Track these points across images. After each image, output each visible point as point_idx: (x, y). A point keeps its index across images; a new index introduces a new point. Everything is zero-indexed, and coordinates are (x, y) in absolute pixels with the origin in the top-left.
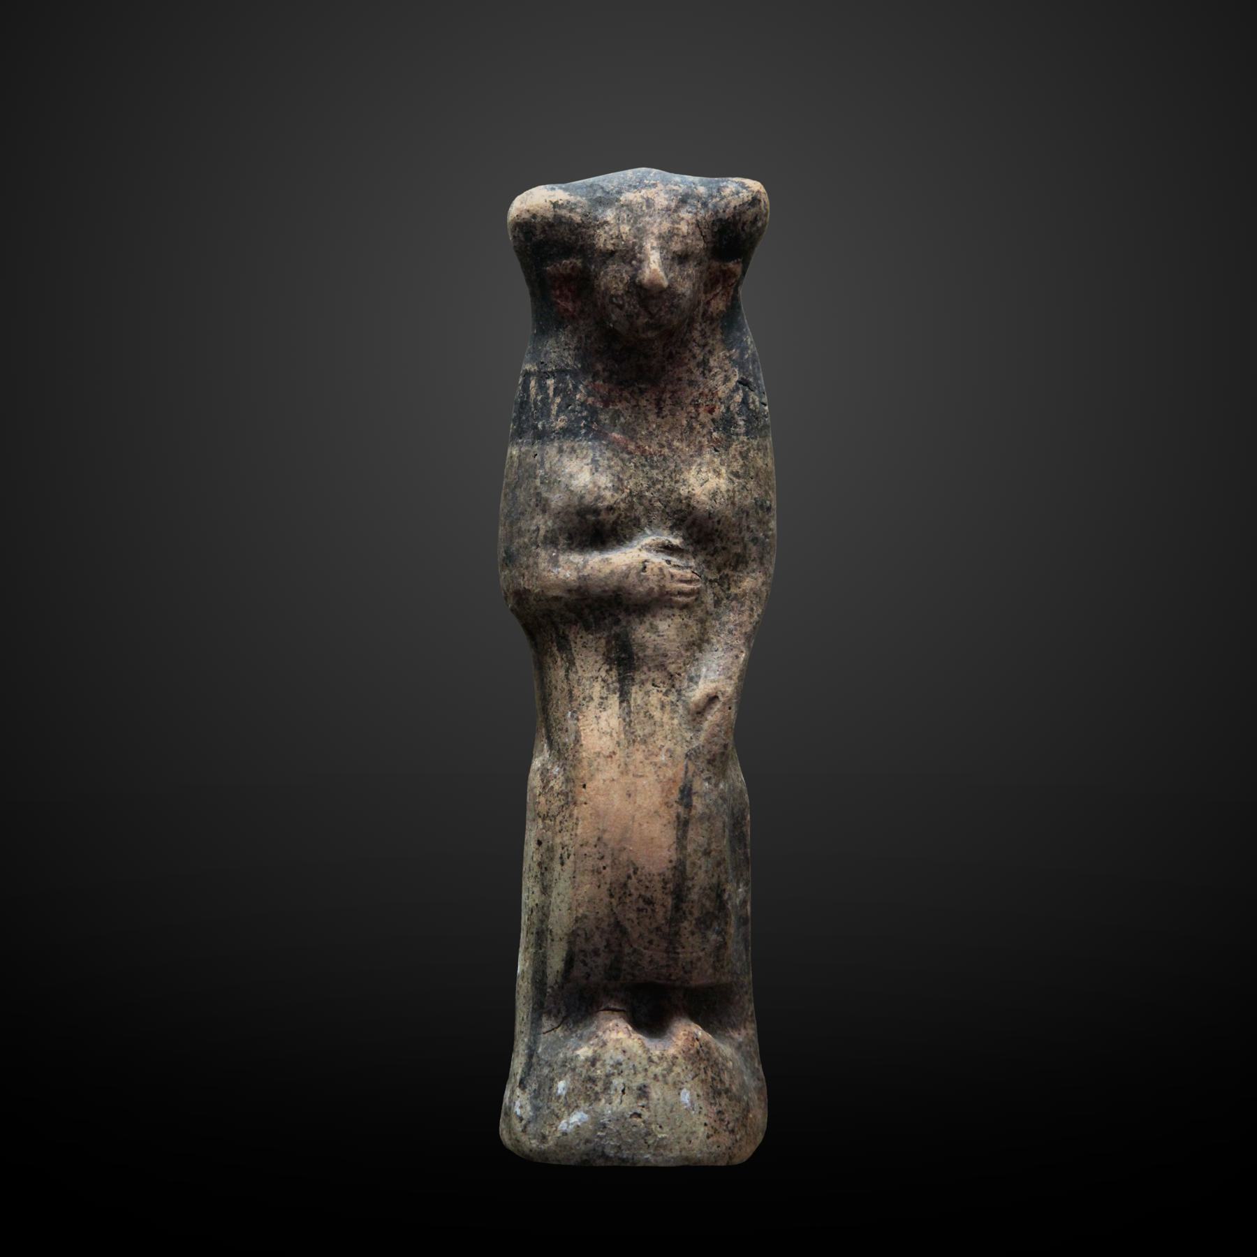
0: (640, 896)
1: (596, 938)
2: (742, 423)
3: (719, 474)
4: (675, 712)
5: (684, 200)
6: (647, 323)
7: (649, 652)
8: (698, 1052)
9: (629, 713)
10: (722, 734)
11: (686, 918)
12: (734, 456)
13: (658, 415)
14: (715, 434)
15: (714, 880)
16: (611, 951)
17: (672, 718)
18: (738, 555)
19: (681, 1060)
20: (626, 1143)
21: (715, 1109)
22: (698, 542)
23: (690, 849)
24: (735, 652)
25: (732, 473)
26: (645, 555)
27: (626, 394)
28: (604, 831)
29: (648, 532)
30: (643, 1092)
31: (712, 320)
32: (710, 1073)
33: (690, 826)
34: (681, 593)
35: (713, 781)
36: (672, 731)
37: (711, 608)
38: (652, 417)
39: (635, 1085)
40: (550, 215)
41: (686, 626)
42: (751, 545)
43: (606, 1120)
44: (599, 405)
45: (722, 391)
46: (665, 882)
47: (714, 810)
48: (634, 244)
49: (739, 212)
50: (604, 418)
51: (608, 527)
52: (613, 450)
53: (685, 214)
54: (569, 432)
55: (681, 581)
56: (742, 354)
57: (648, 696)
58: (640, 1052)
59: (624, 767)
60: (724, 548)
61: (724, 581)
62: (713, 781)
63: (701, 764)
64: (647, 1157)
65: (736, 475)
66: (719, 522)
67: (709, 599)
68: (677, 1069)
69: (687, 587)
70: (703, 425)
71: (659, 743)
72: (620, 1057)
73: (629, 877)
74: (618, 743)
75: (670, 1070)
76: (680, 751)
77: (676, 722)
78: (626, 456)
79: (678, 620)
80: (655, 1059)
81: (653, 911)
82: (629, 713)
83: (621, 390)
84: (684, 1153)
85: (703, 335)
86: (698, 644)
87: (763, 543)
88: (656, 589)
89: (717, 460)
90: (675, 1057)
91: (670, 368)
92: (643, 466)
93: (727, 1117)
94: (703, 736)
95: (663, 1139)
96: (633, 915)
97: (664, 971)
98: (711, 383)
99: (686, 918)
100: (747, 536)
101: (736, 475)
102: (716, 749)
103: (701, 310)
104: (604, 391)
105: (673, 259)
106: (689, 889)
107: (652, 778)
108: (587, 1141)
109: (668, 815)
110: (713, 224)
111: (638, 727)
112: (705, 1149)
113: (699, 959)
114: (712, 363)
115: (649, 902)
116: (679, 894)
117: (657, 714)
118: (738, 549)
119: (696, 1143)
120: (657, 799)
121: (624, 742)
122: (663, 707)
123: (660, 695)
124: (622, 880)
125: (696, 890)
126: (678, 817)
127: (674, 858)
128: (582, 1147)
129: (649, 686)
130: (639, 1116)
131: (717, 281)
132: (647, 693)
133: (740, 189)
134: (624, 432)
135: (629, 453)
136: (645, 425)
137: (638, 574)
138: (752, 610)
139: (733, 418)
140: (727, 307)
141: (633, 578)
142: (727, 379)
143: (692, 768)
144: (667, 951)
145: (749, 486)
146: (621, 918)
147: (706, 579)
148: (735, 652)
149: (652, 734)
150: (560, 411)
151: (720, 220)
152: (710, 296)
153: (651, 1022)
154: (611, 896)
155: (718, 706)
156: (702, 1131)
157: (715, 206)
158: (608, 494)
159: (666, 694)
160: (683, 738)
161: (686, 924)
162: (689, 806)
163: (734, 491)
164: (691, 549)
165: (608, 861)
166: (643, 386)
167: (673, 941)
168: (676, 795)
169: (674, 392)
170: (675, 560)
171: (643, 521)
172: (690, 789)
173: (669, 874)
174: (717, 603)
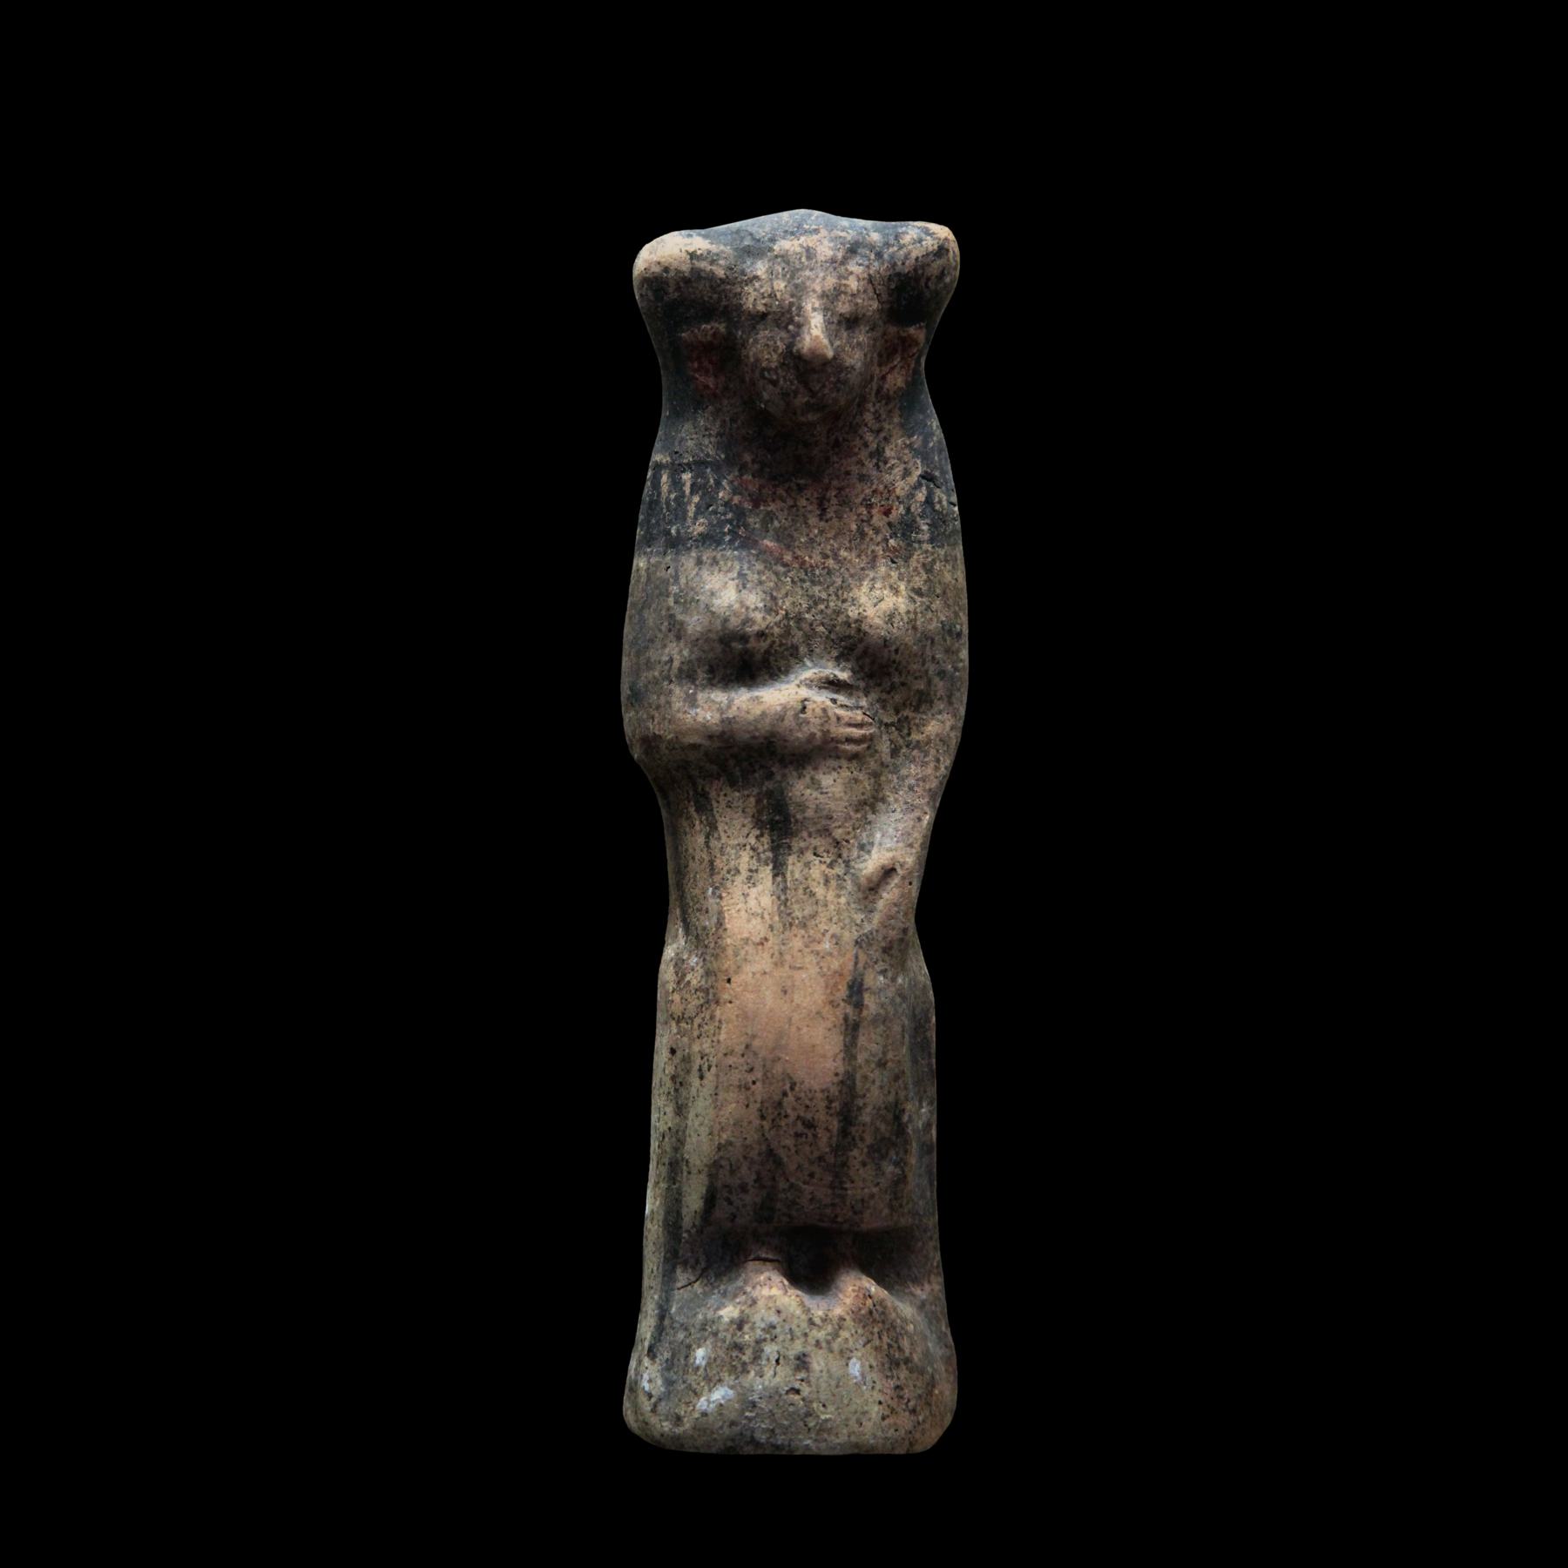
0: (799, 1117)
1: (744, 1170)
2: (925, 528)
3: (896, 592)
4: (842, 888)
6: (807, 403)
7: (810, 813)
8: (871, 1312)
9: (785, 890)
10: (900, 916)
11: (855, 1145)
12: (916, 569)
13: (821, 517)
14: (892, 542)
15: (891, 1098)
16: (762, 1187)
17: (839, 896)
18: (920, 692)
19: (849, 1322)
20: (781, 1426)
21: (892, 1383)
22: (870, 676)
23: (861, 1058)
24: (917, 813)
25: (913, 590)
26: (804, 692)
27: (780, 491)
28: (754, 1037)
29: (808, 663)
30: (802, 1362)
31: (888, 399)
32: (885, 1339)
33: (861, 1030)
34: (849, 740)
35: (890, 974)
36: (839, 912)
37: (887, 758)
38: (813, 520)
39: (792, 1354)
40: (686, 268)
41: (856, 781)
42: (936, 680)
43: (755, 1397)
44: (748, 506)
45: (901, 487)
46: (830, 1100)
47: (891, 1010)
48: (791, 304)
49: (922, 264)
50: (754, 521)
51: (758, 657)
52: (765, 561)
53: (854, 267)
54: (710, 539)
55: (850, 725)
56: (925, 442)
57: (808, 868)
58: (798, 1312)
60: (903, 684)
61: (903, 725)
62: (890, 974)
63: (875, 953)
64: (807, 1443)
65: (919, 592)
66: (897, 651)
67: (884, 747)
68: (844, 1334)
69: (856, 732)
70: (877, 531)
71: (823, 927)
72: (774, 1319)
73: (785, 1094)
74: (771, 927)
75: (836, 1335)
76: (849, 936)
77: (843, 900)
78: (781, 569)
79: (846, 774)
80: (817, 1321)
81: (815, 1136)
82: (785, 890)
83: (775, 486)
84: (853, 1439)
85: (878, 418)
86: (870, 804)
87: (952, 677)
88: (819, 734)
89: (894, 574)
90: (842, 1319)
91: (835, 459)
92: (803, 581)
93: (906, 1393)
94: (877, 918)
95: (827, 1420)
96: (789, 1142)
97: (828, 1211)
98: (888, 478)
99: (855, 1145)
100: (932, 668)
101: (919, 592)
102: (893, 934)
103: (875, 387)
104: (753, 488)
105: (839, 323)
106: (859, 1109)
107: (814, 970)
108: (733, 1423)
109: (834, 1017)
110: (890, 279)
111: (796, 907)
112: (879, 1433)
113: (872, 1196)
114: (888, 453)
115: (810, 1125)
116: (847, 1116)
117: (820, 891)
118: (921, 685)
119: (868, 1426)
120: (819, 996)
121: (779, 926)
122: (827, 881)
123: (824, 867)
124: (776, 1098)
125: (868, 1110)
126: (846, 1019)
127: (841, 1070)
128: (727, 1431)
129: (809, 856)
130: (798, 1392)
131: (895, 351)
132: (808, 865)
134: (778, 539)
135: (785, 565)
136: (805, 530)
137: (796, 716)
138: (938, 760)
139: (914, 521)
140: (907, 382)
141: (789, 722)
142: (907, 473)
143: (863, 958)
144: (832, 1186)
145: (934, 607)
146: (774, 1145)
147: (881, 722)
148: (917, 813)
149: (813, 916)
150: (698, 512)
151: (899, 274)
152: (885, 369)
153: (812, 1275)
154: (763, 1117)
155: (896, 880)
156: (875, 1411)
157: (892, 256)
158: (758, 616)
159: (831, 866)
160: (852, 920)
161: (855, 1153)
162: (859, 1006)
163: (915, 613)
164: (862, 684)
165: (759, 1074)
166: (802, 482)
167: (840, 1174)
168: (843, 992)
169: (840, 489)
170: (841, 699)
171: (803, 649)
172: (861, 984)
173: (834, 1090)
174: (895, 752)
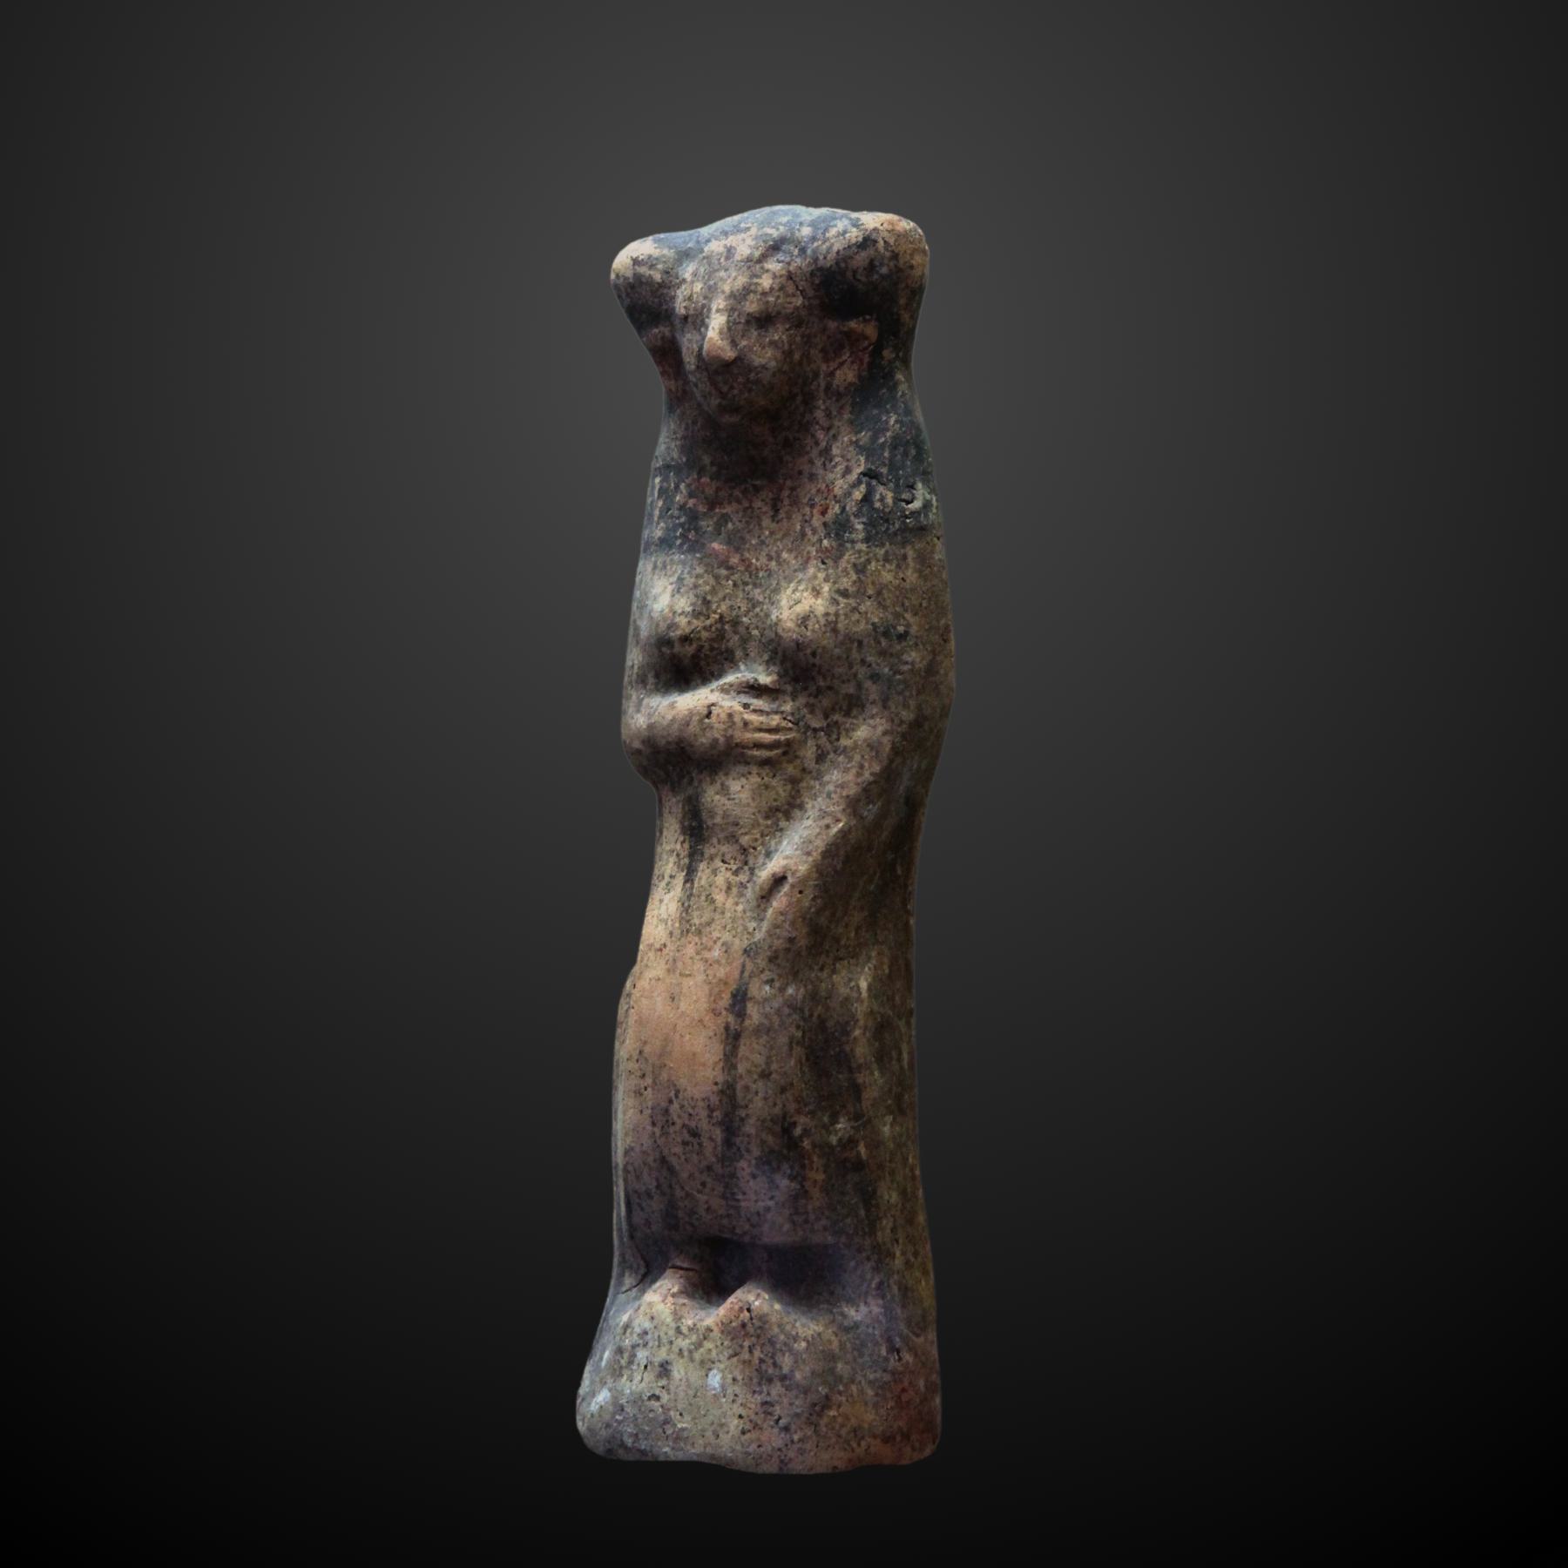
0: (684, 1125)
1: (645, 1176)
2: (860, 527)
3: (817, 592)
4: (741, 895)
5: (775, 247)
6: (720, 405)
7: (718, 820)
8: (744, 1325)
9: (690, 897)
10: (787, 926)
11: (742, 1156)
12: (845, 570)
13: (773, 517)
14: (825, 542)
15: (777, 1110)
16: (663, 1194)
17: (737, 904)
18: (849, 697)
19: (716, 1334)
20: (643, 1431)
21: (759, 1398)
22: (796, 680)
23: (741, 1069)
24: (828, 820)
25: (839, 592)
26: (714, 697)
27: (737, 493)
28: (645, 1043)
29: (742, 667)
30: (664, 1370)
31: (839, 395)
32: (757, 1353)
33: (742, 1041)
34: (758, 745)
35: (777, 984)
36: (734, 920)
37: (810, 763)
38: (766, 522)
39: (657, 1360)
40: (629, 274)
41: (767, 787)
42: (868, 684)
43: (623, 1401)
44: (702, 509)
45: (840, 486)
46: (711, 1109)
47: (776, 1019)
48: (704, 306)
49: (844, 258)
50: (707, 525)
51: (686, 661)
52: (707, 565)
53: (773, 265)
54: (665, 543)
55: (760, 730)
56: (874, 438)
57: (716, 876)
58: (669, 1320)
59: (692, 958)
60: (830, 688)
61: (833, 730)
62: (777, 984)
63: (762, 962)
64: (666, 1450)
65: (844, 594)
66: (814, 654)
67: (809, 752)
68: (708, 1345)
69: (768, 738)
70: (814, 531)
71: (716, 934)
72: (647, 1325)
73: (671, 1101)
74: (671, 934)
75: (699, 1345)
76: (739, 944)
77: (740, 908)
78: (724, 572)
79: (755, 779)
80: (684, 1330)
81: (700, 1145)
82: (690, 897)
83: (732, 488)
84: (709, 1450)
85: (829, 415)
86: (782, 812)
87: (890, 680)
88: (722, 740)
89: (821, 575)
90: (709, 1330)
91: (788, 458)
92: (746, 584)
93: (777, 1410)
94: (765, 925)
95: (683, 1429)
96: (678, 1150)
97: (725, 1222)
98: (831, 476)
99: (742, 1156)
100: (862, 672)
101: (844, 594)
102: (778, 943)
103: (823, 385)
104: (710, 491)
105: (748, 322)
106: (742, 1120)
107: (700, 978)
108: (608, 1426)
109: (714, 1025)
110: (812, 274)
111: (696, 914)
112: (738, 1447)
113: (768, 1209)
114: (835, 451)
115: (695, 1134)
116: (730, 1126)
117: (719, 898)
118: (850, 689)
119: (725, 1440)
120: (704, 1005)
121: (677, 932)
122: (729, 888)
123: (729, 874)
124: (664, 1104)
125: (752, 1121)
126: (727, 1028)
127: (720, 1079)
128: (604, 1433)
129: (718, 863)
130: (658, 1398)
131: (842, 347)
132: (715, 872)
133: (837, 227)
134: (729, 542)
135: (729, 568)
136: (756, 532)
137: (701, 721)
138: (862, 767)
139: (848, 520)
140: (860, 377)
141: (694, 728)
142: (848, 471)
143: (749, 966)
144: (723, 1197)
145: (863, 608)
146: (666, 1152)
147: (808, 727)
148: (828, 820)
149: (709, 924)
150: (660, 517)
151: (821, 269)
152: (833, 365)
153: (711, 1284)
154: (654, 1124)
155: (786, 888)
156: (734, 1424)
157: (814, 251)
158: (683, 621)
159: (736, 873)
160: (746, 928)
161: (743, 1164)
162: (741, 1015)
163: (837, 615)
164: (789, 688)
165: (649, 1081)
166: (758, 483)
167: (729, 1182)
168: (726, 999)
169: (793, 489)
170: (757, 703)
171: (739, 653)
172: (745, 993)
173: (715, 1100)
174: (821, 758)
